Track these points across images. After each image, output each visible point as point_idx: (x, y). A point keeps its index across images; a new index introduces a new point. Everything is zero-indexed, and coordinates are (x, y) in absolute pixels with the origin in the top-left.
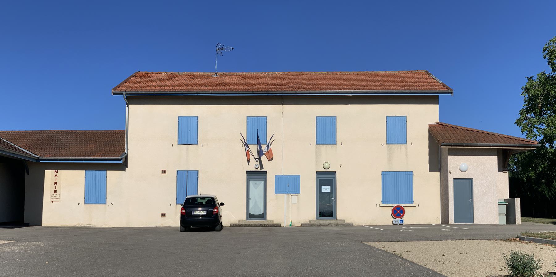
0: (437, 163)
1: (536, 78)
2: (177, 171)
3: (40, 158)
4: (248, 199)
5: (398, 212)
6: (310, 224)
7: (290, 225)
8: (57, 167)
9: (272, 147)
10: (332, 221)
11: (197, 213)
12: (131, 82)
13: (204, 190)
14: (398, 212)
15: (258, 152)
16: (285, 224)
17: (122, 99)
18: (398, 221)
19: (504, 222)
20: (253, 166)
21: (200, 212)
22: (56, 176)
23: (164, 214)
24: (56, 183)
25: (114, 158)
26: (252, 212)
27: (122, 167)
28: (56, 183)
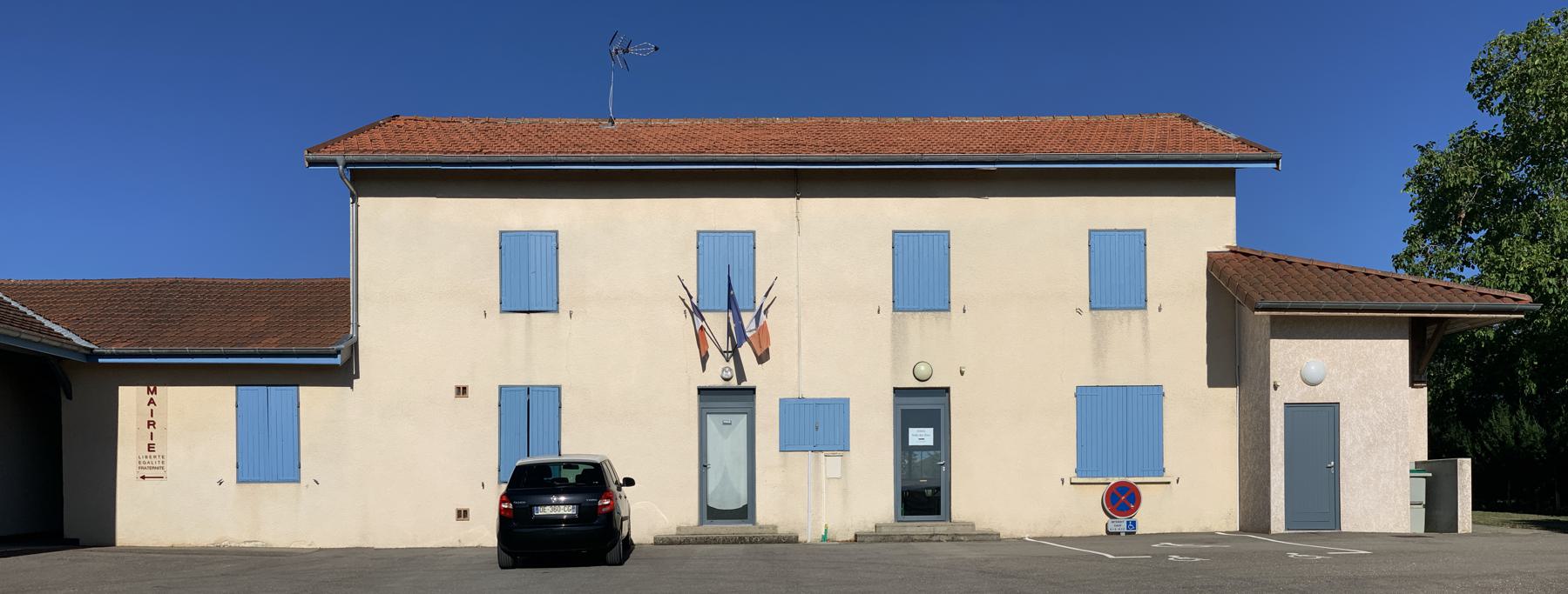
0: (1231, 360)
1: (1443, 146)
2: (501, 388)
3: (97, 349)
4: (703, 467)
5: (1122, 500)
6: (879, 537)
7: (824, 538)
8: (154, 376)
9: (770, 320)
10: (941, 528)
11: (548, 511)
12: (366, 137)
13: (577, 444)
14: (1122, 500)
15: (730, 333)
16: (808, 536)
17: (336, 179)
18: (1121, 524)
19: (1421, 530)
20: (717, 373)
21: (560, 508)
22: (151, 402)
23: (466, 512)
24: (151, 424)
25: (312, 348)
26: (714, 503)
27: (344, 373)
28: (151, 424)
